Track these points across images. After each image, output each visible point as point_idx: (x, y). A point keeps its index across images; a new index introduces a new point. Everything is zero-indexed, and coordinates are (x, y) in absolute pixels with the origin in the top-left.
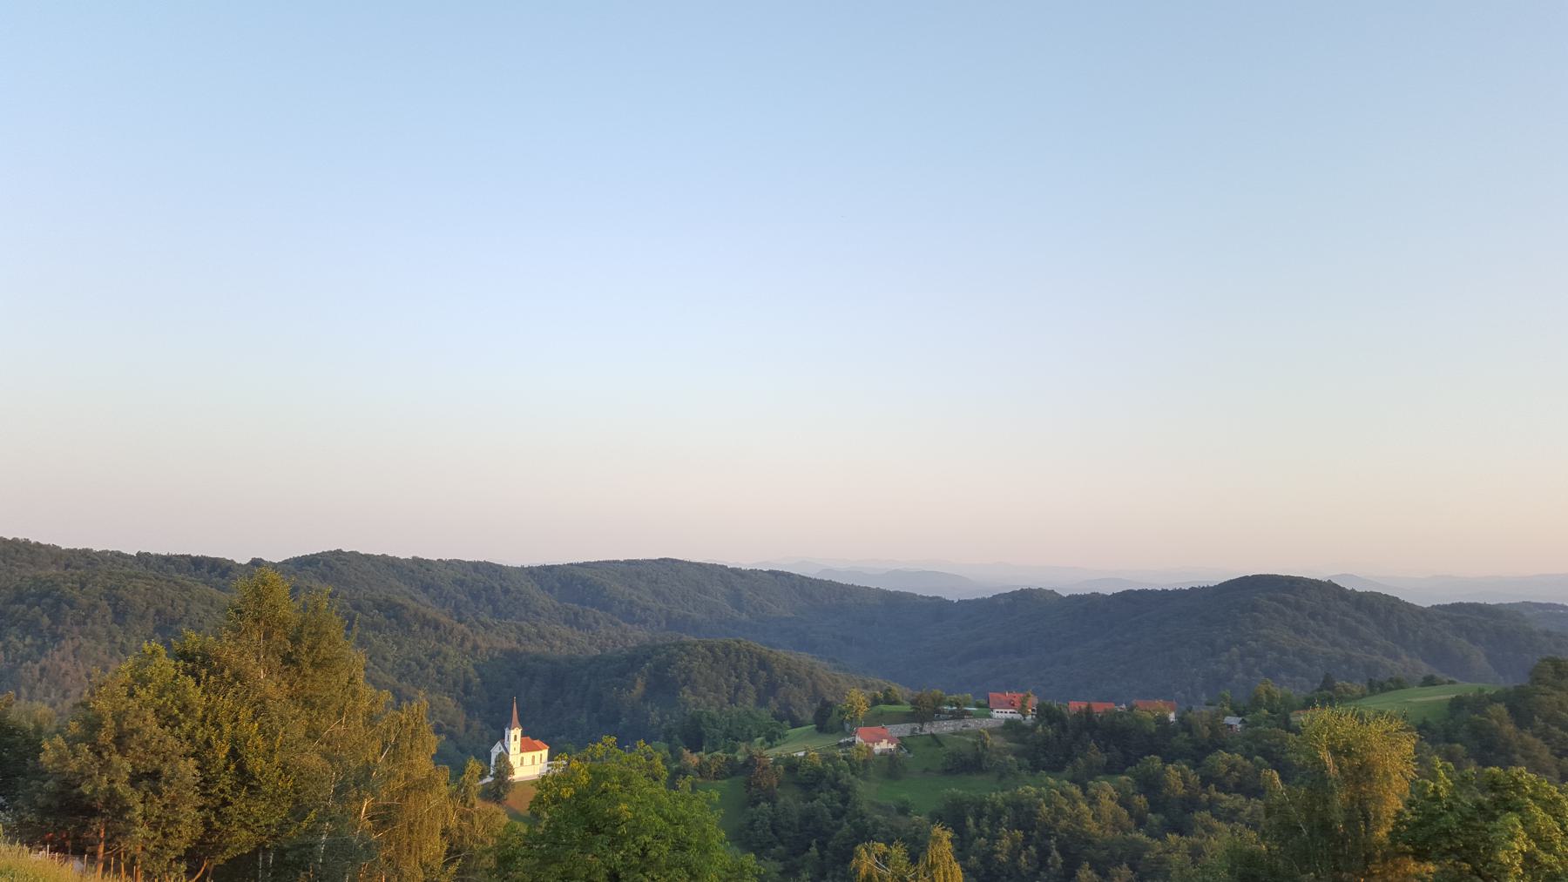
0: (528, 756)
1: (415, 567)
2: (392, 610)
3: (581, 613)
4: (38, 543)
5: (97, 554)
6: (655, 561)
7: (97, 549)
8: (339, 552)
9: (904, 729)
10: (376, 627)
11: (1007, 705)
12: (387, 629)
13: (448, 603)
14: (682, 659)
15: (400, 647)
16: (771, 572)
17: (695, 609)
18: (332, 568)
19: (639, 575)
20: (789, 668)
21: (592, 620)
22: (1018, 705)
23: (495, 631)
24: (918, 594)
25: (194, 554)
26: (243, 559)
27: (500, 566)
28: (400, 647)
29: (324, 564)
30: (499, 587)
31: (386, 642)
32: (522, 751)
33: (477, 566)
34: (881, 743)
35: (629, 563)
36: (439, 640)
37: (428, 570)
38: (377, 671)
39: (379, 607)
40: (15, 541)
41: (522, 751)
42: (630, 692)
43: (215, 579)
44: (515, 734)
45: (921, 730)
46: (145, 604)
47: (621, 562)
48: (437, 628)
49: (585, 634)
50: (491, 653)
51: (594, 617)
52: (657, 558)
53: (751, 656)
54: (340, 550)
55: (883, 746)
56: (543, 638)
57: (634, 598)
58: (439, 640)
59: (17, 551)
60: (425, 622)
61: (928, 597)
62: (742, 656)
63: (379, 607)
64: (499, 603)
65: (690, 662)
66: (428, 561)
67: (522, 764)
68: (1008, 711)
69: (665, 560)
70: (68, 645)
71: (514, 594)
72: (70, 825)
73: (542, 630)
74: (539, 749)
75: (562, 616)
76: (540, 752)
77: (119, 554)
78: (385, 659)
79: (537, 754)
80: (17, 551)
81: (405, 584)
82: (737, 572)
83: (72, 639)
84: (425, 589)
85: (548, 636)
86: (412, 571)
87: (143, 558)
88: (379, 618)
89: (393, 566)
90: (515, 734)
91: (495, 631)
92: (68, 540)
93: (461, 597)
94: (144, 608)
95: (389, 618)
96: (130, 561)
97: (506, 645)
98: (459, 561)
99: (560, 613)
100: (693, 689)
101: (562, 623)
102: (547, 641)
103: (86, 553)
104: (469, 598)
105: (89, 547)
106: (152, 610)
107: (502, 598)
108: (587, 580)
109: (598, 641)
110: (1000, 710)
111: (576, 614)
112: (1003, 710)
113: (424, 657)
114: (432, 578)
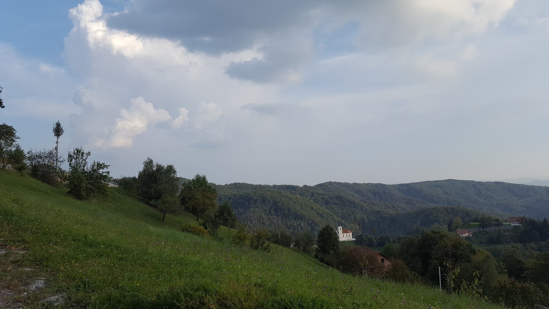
0: (345, 235)
2: (339, 198)
4: (248, 184)
5: (262, 186)
7: (263, 184)
8: (215, 184)
9: (476, 230)
11: (517, 221)
16: (495, 182)
18: (326, 187)
19: (437, 186)
22: (520, 221)
25: (287, 185)
30: (382, 192)
32: (343, 233)
33: (376, 185)
35: (434, 181)
36: (355, 207)
37: (359, 186)
40: (242, 183)
41: (343, 233)
45: (483, 230)
46: (270, 198)
47: (432, 181)
52: (446, 179)
55: (467, 235)
56: (394, 208)
59: (243, 186)
64: (382, 197)
66: (359, 184)
67: (343, 236)
68: (517, 223)
70: (252, 210)
71: (387, 194)
72: (342, 258)
74: (348, 233)
76: (349, 234)
77: (268, 186)
78: (338, 213)
79: (348, 234)
80: (243, 186)
81: (351, 191)
82: (480, 183)
83: (253, 208)
84: (358, 193)
86: (353, 187)
87: (274, 186)
89: (347, 186)
90: (340, 229)
92: (255, 182)
94: (269, 199)
96: (271, 188)
98: (370, 183)
102: (396, 209)
103: (260, 186)
105: (265, 184)
107: (383, 195)
108: (416, 188)
111: (410, 200)
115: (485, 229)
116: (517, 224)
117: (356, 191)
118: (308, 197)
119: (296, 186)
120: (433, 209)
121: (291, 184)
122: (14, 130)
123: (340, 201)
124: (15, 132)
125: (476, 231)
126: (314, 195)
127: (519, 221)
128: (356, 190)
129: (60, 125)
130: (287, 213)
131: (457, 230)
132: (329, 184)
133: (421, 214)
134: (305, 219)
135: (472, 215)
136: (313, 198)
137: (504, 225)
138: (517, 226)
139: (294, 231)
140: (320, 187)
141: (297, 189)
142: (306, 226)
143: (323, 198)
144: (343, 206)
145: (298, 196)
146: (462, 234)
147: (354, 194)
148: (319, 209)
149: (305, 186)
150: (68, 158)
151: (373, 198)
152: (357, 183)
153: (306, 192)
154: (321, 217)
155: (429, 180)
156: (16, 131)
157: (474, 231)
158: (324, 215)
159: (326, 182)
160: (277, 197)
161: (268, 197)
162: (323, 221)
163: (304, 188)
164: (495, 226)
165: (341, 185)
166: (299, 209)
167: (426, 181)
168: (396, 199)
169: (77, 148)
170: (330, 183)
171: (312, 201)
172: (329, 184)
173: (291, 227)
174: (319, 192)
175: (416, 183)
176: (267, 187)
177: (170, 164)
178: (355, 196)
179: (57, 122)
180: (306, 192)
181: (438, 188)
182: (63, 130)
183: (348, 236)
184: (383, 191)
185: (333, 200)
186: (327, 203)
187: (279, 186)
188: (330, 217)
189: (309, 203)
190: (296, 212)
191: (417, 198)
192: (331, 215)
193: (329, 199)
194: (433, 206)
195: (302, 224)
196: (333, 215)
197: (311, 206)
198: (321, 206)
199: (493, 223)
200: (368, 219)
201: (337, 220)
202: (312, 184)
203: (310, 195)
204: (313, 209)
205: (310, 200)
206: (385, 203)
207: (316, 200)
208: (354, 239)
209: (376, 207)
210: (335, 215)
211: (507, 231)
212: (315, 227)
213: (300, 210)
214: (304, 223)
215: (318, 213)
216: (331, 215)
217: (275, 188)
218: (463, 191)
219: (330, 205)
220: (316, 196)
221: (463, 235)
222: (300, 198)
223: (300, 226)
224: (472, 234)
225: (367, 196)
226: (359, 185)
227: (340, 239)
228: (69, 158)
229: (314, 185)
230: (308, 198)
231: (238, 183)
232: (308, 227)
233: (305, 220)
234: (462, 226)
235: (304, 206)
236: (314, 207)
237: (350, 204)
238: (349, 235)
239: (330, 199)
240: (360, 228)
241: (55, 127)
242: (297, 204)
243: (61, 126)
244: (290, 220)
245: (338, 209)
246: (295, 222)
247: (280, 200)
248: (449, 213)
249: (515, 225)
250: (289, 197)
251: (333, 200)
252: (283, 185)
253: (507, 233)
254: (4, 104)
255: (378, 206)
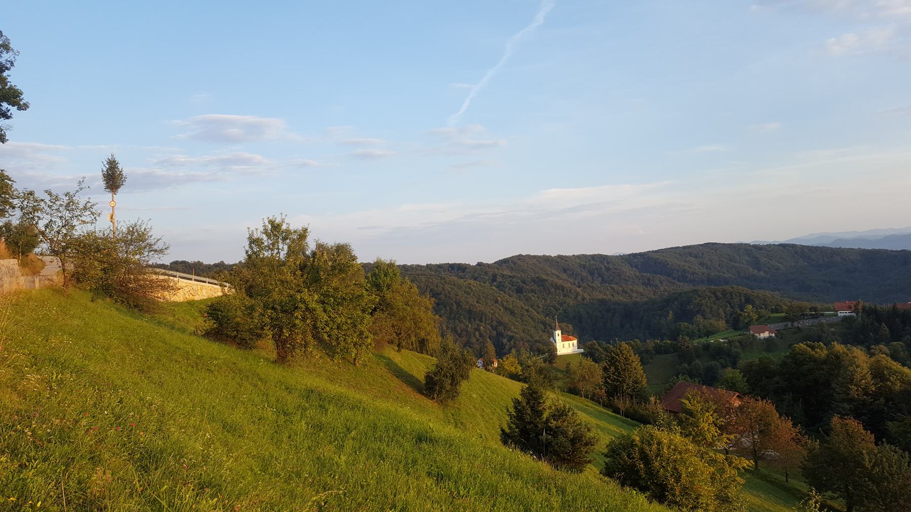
0: (566, 343)
1: (559, 260)
2: (540, 282)
3: (652, 278)
5: (408, 266)
6: (701, 245)
7: (409, 264)
8: (520, 255)
9: (780, 326)
10: (533, 291)
12: (539, 292)
13: (577, 277)
14: (696, 299)
15: (546, 300)
16: (781, 245)
17: (728, 271)
18: (515, 264)
20: (766, 301)
21: (658, 282)
22: (853, 308)
23: (598, 291)
24: (890, 249)
26: (473, 263)
27: (606, 256)
28: (546, 300)
29: (512, 262)
30: (604, 268)
31: (539, 298)
32: (562, 341)
33: (593, 257)
34: (765, 334)
35: (684, 247)
36: (565, 296)
38: (534, 313)
39: (533, 281)
41: (562, 341)
42: (666, 319)
43: (460, 274)
44: (558, 333)
45: (792, 325)
46: (425, 287)
47: (681, 248)
48: (563, 290)
49: (651, 289)
50: (592, 301)
51: (660, 281)
53: (740, 296)
54: (521, 255)
55: (766, 335)
56: (626, 293)
57: (686, 268)
58: (565, 296)
60: (557, 287)
61: (896, 251)
62: (734, 296)
63: (533, 281)
64: (604, 276)
65: (701, 301)
66: (566, 257)
69: (708, 243)
73: (625, 288)
75: (641, 281)
77: (418, 266)
78: (538, 307)
79: (571, 342)
81: (555, 269)
84: (565, 271)
85: (629, 292)
86: (557, 262)
87: (429, 267)
88: (535, 287)
90: (558, 333)
91: (598, 291)
93: (584, 274)
95: (539, 287)
96: (423, 269)
97: (601, 296)
98: (583, 255)
99: (640, 279)
100: (703, 315)
101: (641, 285)
102: (629, 294)
104: (589, 275)
106: (428, 290)
109: (659, 293)
110: (841, 312)
111: (649, 279)
112: (844, 312)
113: (557, 305)
114: (568, 265)
115: (796, 324)
116: (847, 314)
117: (562, 268)
118: (487, 282)
119: (465, 264)
120: (692, 292)
121: (458, 262)
122: (10, 180)
123: (541, 287)
124: (10, 183)
125: (780, 328)
126: (496, 277)
127: (851, 308)
128: (563, 267)
129: (117, 163)
130: (456, 309)
131: (751, 327)
132: (519, 259)
133: (673, 302)
134: (486, 318)
135: (756, 299)
136: (495, 283)
137: (826, 316)
138: (848, 316)
139: (468, 340)
140: (503, 264)
141: (467, 270)
142: (488, 332)
143: (513, 283)
144: (545, 294)
145: (472, 282)
146: (759, 333)
147: (558, 274)
148: (507, 301)
149: (480, 264)
150: (247, 248)
151: (590, 278)
152: (562, 256)
153: (483, 274)
154: (511, 313)
155: (676, 246)
156: (13, 181)
157: (778, 329)
158: (517, 312)
159: (513, 256)
160: (437, 285)
161: (423, 285)
162: (516, 321)
163: (478, 267)
164: (811, 318)
165: (537, 260)
166: (475, 303)
167: (672, 248)
168: (627, 278)
169: (271, 218)
170: (520, 257)
171: (495, 288)
172: (519, 259)
173: (464, 332)
174: (505, 273)
175: (656, 251)
176: (417, 268)
177: (342, 241)
178: (562, 277)
179: (110, 158)
180: (483, 274)
181: (691, 258)
182: (124, 175)
183: (571, 345)
184: (605, 266)
185: (529, 285)
186: (519, 291)
187: (437, 265)
188: (525, 314)
189: (491, 292)
190: (470, 308)
191: (659, 276)
192: (527, 311)
193: (522, 284)
194: (686, 287)
195: (482, 328)
196: (531, 309)
197: (493, 296)
198: (510, 296)
199: (808, 312)
200: (588, 313)
201: (538, 319)
202: (491, 261)
203: (491, 279)
204: (497, 302)
205: (490, 287)
206: (611, 285)
207: (500, 287)
208: (582, 350)
209: (597, 294)
210: (533, 311)
211: (832, 325)
212: (503, 331)
213: (477, 304)
214: (484, 325)
215: (506, 309)
216: (527, 311)
217: (430, 269)
218: (731, 261)
219: (525, 293)
220: (499, 279)
221: (760, 335)
222: (475, 285)
223: (479, 332)
224: (775, 334)
225: (580, 276)
226: (567, 259)
227: (558, 350)
228: (251, 247)
229: (494, 262)
230: (488, 284)
231: (368, 263)
232: (491, 332)
233: (486, 321)
234: (757, 320)
235: (483, 297)
236: (499, 298)
237: (558, 290)
238: (573, 345)
239: (524, 285)
240: (574, 329)
241: (105, 169)
242: (471, 294)
243: (120, 167)
244: (460, 322)
245: (537, 299)
246: (470, 325)
247: (443, 289)
248: (718, 299)
249: (845, 316)
250: (456, 283)
251: (529, 285)
252: (443, 264)
253: (833, 329)
254: (25, 98)
255: (600, 292)
